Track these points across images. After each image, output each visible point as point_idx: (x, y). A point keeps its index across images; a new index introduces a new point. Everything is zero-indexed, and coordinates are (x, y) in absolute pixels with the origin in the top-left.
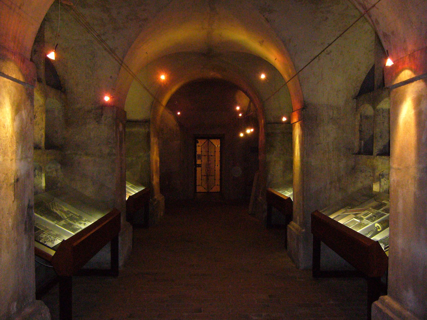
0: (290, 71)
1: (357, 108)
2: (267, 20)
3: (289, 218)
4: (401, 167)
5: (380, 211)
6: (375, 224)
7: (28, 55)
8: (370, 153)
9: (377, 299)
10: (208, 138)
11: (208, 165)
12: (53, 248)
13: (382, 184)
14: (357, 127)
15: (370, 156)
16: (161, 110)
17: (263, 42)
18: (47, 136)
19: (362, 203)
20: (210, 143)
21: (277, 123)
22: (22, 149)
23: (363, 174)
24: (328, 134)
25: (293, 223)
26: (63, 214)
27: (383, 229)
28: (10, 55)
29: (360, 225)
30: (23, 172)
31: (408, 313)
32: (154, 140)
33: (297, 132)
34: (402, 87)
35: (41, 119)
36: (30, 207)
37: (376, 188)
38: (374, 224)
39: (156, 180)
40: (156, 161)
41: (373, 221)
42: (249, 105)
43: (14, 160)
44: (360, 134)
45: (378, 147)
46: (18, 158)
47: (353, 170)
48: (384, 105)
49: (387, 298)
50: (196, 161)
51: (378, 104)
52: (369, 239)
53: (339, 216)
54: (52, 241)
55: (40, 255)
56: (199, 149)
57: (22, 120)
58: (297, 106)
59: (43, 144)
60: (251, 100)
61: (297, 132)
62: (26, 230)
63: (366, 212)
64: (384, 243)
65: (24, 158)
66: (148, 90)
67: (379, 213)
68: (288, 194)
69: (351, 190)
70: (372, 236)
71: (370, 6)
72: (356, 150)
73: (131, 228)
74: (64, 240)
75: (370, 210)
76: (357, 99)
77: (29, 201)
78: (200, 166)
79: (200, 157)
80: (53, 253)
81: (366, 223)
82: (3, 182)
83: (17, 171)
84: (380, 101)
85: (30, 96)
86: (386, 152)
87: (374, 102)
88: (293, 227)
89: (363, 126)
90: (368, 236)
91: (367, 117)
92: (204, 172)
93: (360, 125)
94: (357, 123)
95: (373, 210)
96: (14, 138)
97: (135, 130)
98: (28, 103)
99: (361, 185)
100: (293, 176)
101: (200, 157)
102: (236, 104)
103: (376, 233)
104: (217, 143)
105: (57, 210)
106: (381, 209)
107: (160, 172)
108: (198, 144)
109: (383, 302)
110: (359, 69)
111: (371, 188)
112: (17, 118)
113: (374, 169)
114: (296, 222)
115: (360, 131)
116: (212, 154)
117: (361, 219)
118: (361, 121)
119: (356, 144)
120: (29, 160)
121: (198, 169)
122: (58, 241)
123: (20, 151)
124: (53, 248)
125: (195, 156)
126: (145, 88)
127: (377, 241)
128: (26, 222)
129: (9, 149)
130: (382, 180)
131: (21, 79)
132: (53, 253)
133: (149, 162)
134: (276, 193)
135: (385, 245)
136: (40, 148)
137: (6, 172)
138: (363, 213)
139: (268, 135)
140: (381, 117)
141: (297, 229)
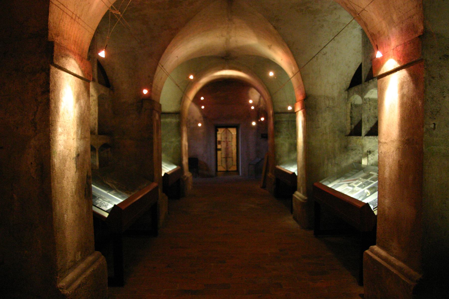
0: (294, 69)
1: (348, 98)
2: (275, 28)
3: (295, 188)
4: (386, 141)
5: (369, 180)
6: (364, 191)
7: (85, 55)
8: (360, 134)
9: (368, 249)
10: (227, 127)
11: (227, 149)
12: (107, 211)
13: (370, 159)
14: (349, 114)
15: (359, 137)
16: (189, 102)
17: (271, 46)
18: (99, 125)
19: (353, 175)
20: (228, 131)
21: (283, 113)
22: (81, 130)
23: (354, 152)
24: (326, 121)
25: (297, 193)
26: (114, 186)
27: (372, 193)
28: (71, 54)
29: (352, 191)
30: (82, 149)
31: (393, 258)
32: (184, 129)
33: (300, 119)
34: (387, 77)
35: (94, 110)
36: (88, 177)
37: (364, 162)
38: (364, 191)
39: (185, 161)
40: (185, 145)
41: (363, 188)
42: (260, 100)
43: (75, 139)
44: (351, 120)
45: (365, 129)
46: (79, 137)
47: (346, 149)
48: (372, 94)
49: (376, 248)
50: (216, 146)
51: (365, 95)
52: (360, 202)
53: (335, 185)
54: (106, 206)
55: (97, 217)
56: (219, 137)
57: (81, 107)
58: (299, 97)
59: (96, 131)
60: (262, 95)
61: (300, 119)
62: (85, 195)
63: (357, 181)
64: (372, 205)
65: (82, 138)
66: (179, 87)
67: (367, 182)
68: (293, 169)
69: (344, 164)
70: (363, 199)
71: (361, 9)
72: (349, 131)
73: (167, 198)
74: (115, 205)
75: (360, 180)
76: (348, 91)
77: (88, 172)
78: (220, 150)
79: (220, 142)
80: (106, 215)
81: (357, 190)
82: (67, 156)
83: (77, 148)
84: (367, 92)
85: (87, 89)
86: (374, 131)
87: (362, 93)
88: (298, 196)
89: (353, 113)
90: (360, 199)
91: (356, 106)
92: (223, 155)
93: (351, 112)
94: (349, 111)
95: (362, 180)
96: (75, 121)
97: (168, 120)
98: (85, 94)
99: (352, 160)
100: (297, 155)
101: (220, 142)
102: (249, 98)
103: (366, 197)
104: (233, 131)
105: (109, 182)
106: (369, 179)
107: (189, 154)
108: (218, 133)
109: (372, 251)
110: (349, 67)
111: (360, 162)
112: (77, 105)
113: (363, 147)
114: (300, 192)
115: (351, 117)
116: (230, 140)
117: (353, 187)
118: (352, 108)
119: (348, 128)
120: (87, 139)
121: (219, 153)
122: (110, 206)
123: (80, 132)
124: (107, 211)
125: (217, 142)
126: (177, 85)
127: (368, 203)
128: (85, 189)
129: (72, 130)
130: (370, 156)
131: (80, 74)
132: (106, 215)
133: (180, 146)
134: (282, 169)
135: (374, 206)
136: (94, 134)
137: (70, 149)
138: (355, 182)
139: (275, 123)
140: (368, 105)
141: (300, 197)
